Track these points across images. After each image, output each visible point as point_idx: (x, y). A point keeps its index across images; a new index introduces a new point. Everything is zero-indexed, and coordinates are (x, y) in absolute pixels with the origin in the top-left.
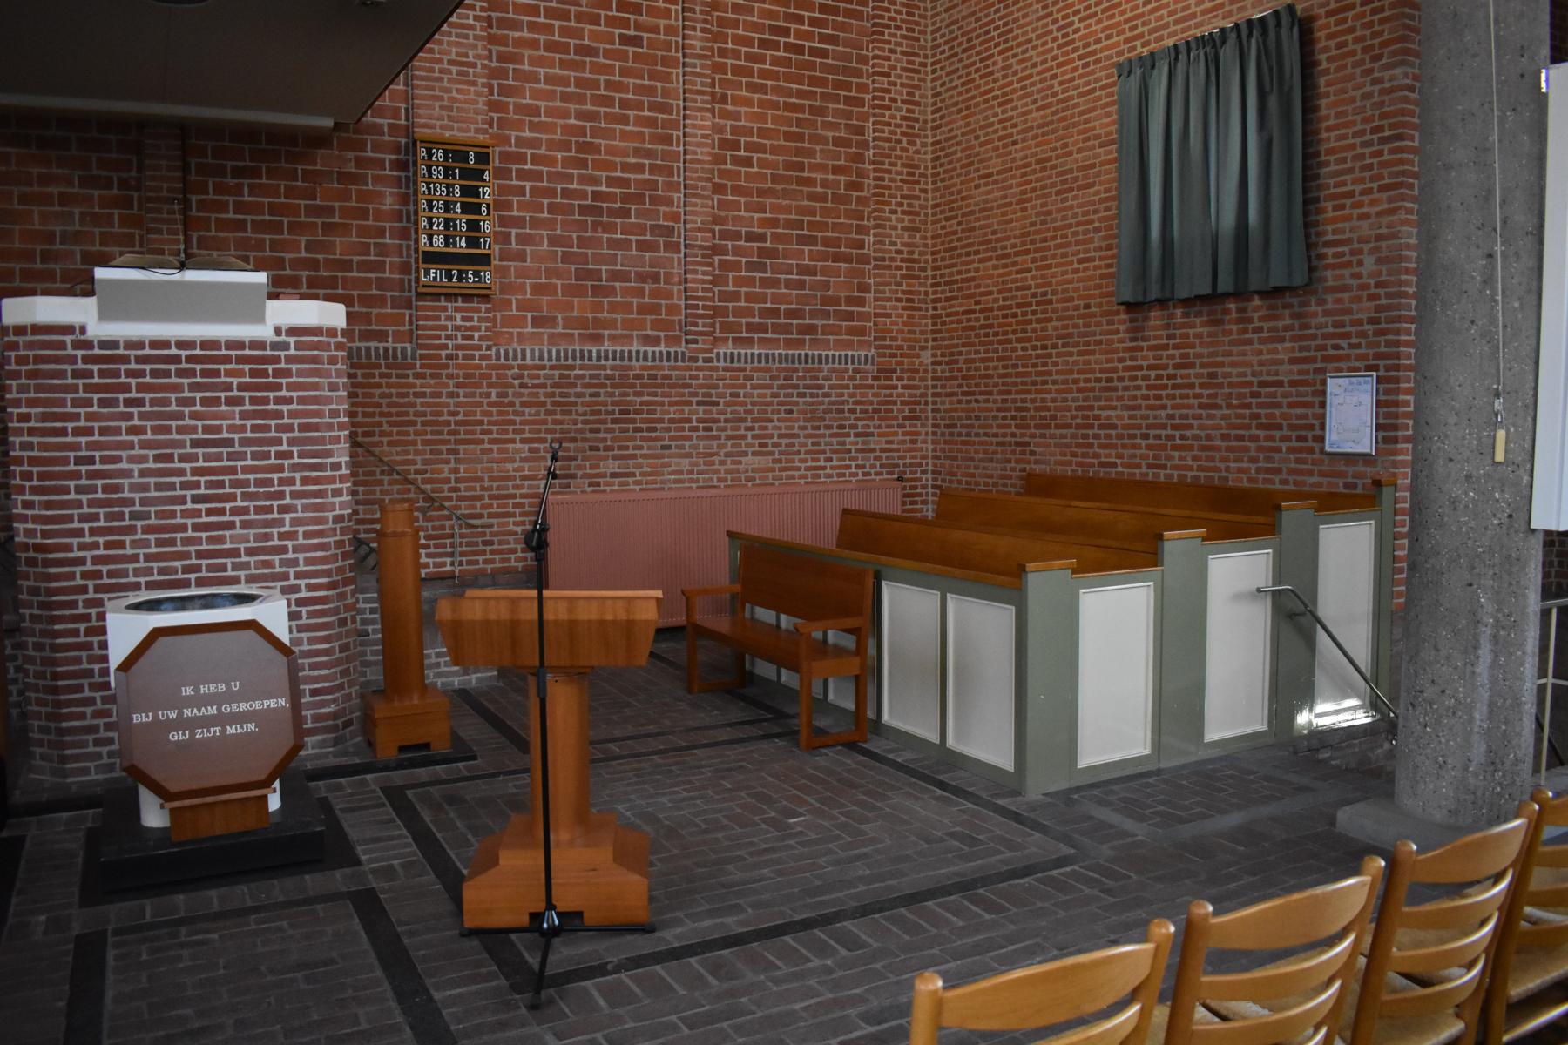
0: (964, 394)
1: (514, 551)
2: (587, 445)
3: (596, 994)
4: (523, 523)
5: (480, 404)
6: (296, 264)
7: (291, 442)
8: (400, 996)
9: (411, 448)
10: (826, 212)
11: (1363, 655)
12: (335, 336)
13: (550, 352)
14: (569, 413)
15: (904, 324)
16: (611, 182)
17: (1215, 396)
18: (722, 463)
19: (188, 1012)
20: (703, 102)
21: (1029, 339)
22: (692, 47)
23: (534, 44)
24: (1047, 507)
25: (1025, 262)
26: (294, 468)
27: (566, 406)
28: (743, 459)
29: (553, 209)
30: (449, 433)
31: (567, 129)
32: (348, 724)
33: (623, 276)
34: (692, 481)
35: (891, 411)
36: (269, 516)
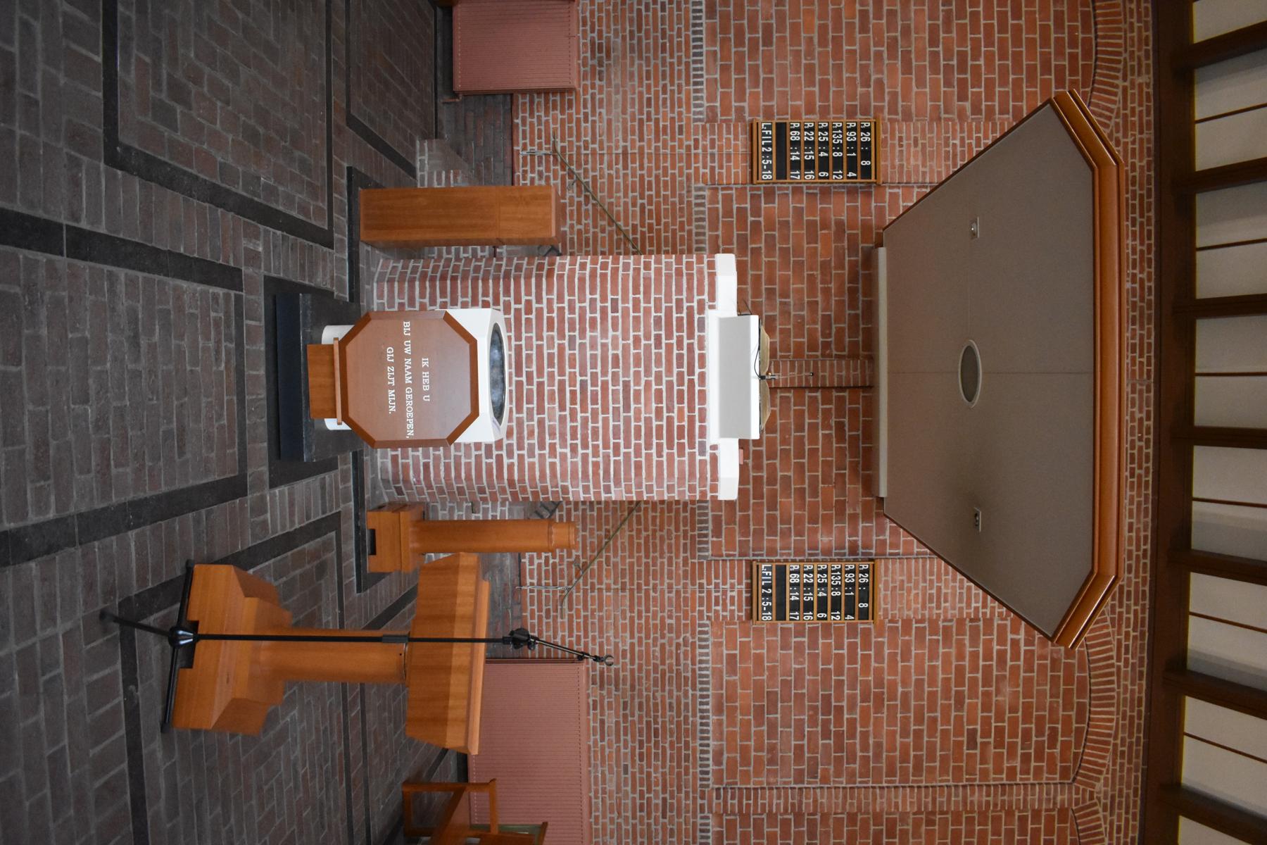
2: (628, 699)
6: (772, 469)
7: (627, 455)
8: (137, 505)
9: (627, 554)
13: (707, 669)
14: (656, 685)
16: (852, 722)
18: (612, 820)
19: (156, 338)
20: (926, 804)
22: (973, 794)
23: (960, 656)
26: (607, 457)
27: (661, 682)
29: (826, 672)
30: (639, 585)
31: (893, 685)
32: (399, 491)
33: (772, 732)
34: (596, 792)
36: (568, 437)
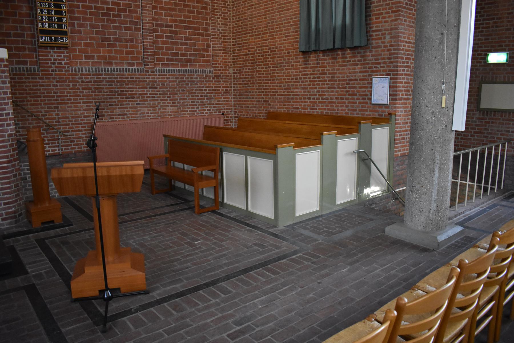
0: (245, 84)
1: (83, 144)
3: (129, 323)
4: (85, 134)
5: (66, 89)
10: (194, 17)
11: (385, 172)
12: (3, 61)
13: (92, 69)
14: (101, 92)
15: (223, 59)
17: (334, 84)
18: (159, 109)
21: (268, 64)
24: (277, 124)
25: (266, 37)
28: (167, 108)
29: (91, 14)
30: (55, 100)
33: (119, 40)
34: (148, 116)
35: (219, 90)
